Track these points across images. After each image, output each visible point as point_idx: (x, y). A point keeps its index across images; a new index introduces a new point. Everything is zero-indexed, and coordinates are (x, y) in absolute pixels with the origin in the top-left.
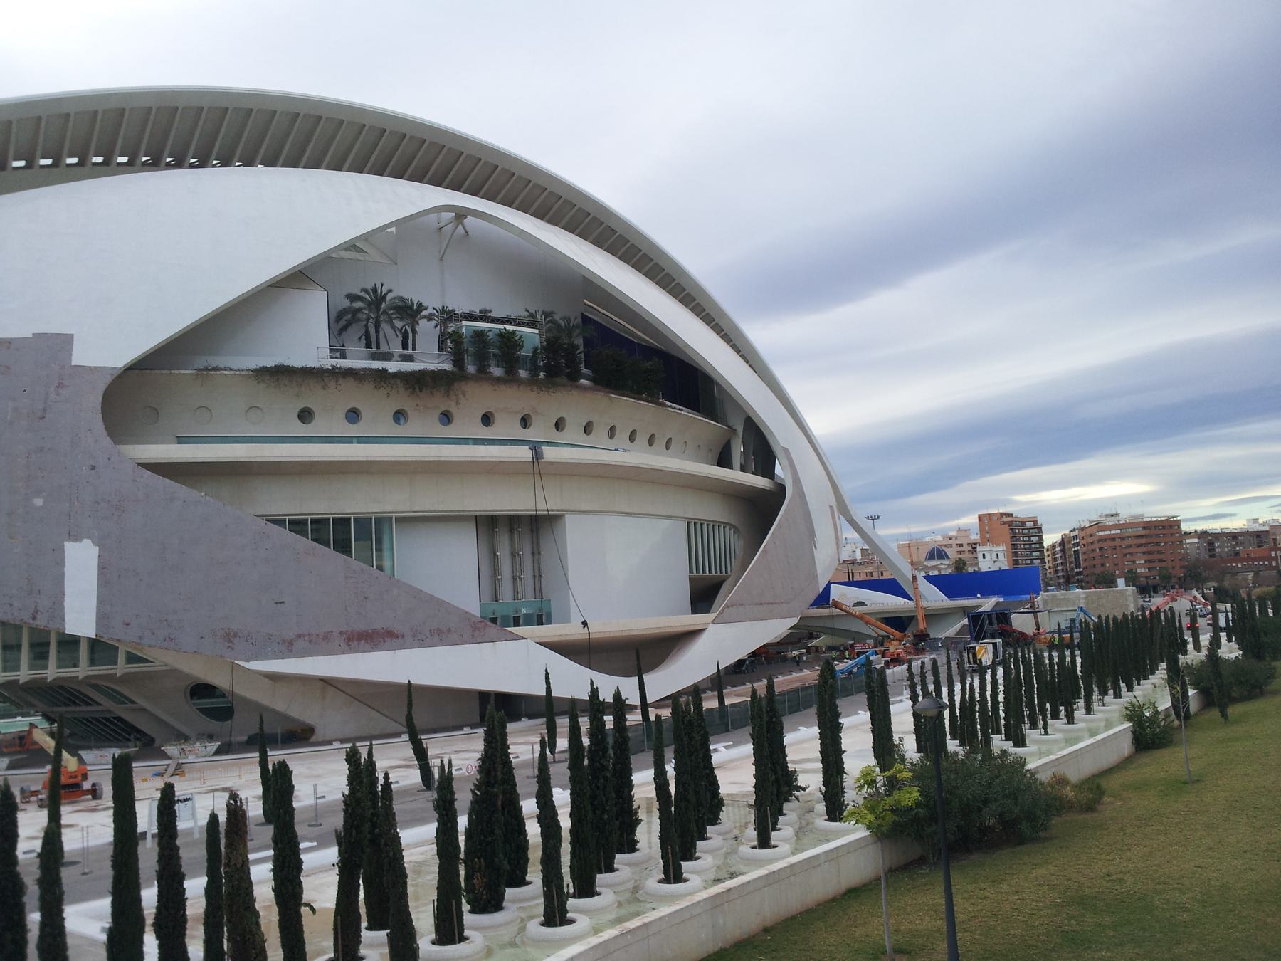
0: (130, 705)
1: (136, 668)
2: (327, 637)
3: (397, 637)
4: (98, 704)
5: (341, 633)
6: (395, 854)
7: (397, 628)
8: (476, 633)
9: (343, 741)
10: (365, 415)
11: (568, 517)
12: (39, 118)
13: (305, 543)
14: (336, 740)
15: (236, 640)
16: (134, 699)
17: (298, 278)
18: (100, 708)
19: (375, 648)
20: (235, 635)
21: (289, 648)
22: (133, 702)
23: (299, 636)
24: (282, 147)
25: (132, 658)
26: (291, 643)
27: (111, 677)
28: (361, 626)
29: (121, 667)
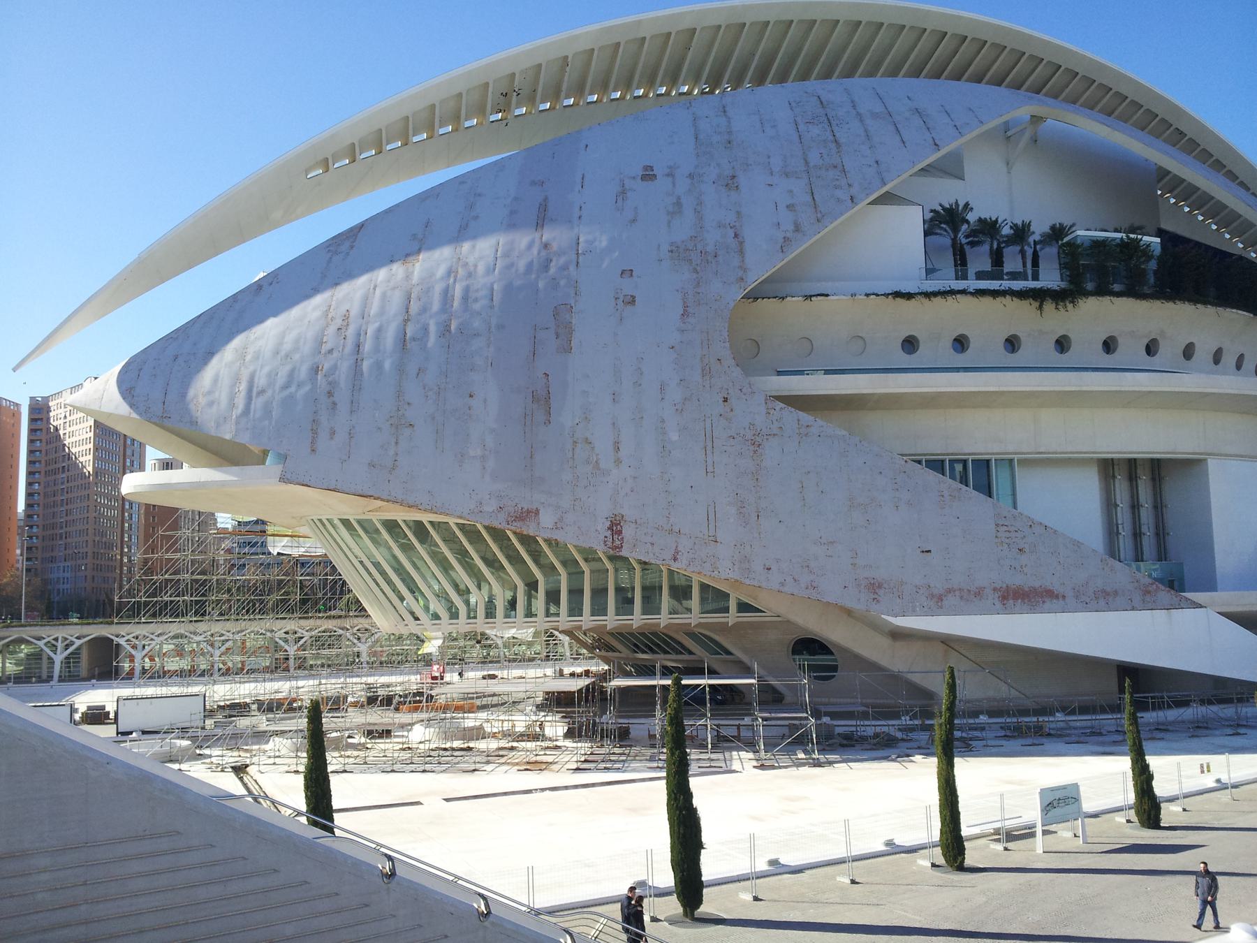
0: (725, 656)
1: (748, 617)
2: (979, 593)
3: (1057, 597)
4: (691, 653)
5: (995, 589)
6: (676, 799)
7: (1057, 588)
8: (1148, 598)
9: (116, 714)
10: (947, 342)
11: (1212, 464)
12: (567, 57)
13: (947, 484)
14: (982, 713)
15: (881, 592)
16: (694, 650)
17: (22, 626)
18: (692, 657)
19: (1033, 609)
20: (880, 586)
21: (938, 602)
22: (728, 653)
23: (949, 591)
24: (780, 46)
25: (744, 607)
26: (940, 598)
27: (723, 628)
28: (1017, 580)
29: (732, 617)
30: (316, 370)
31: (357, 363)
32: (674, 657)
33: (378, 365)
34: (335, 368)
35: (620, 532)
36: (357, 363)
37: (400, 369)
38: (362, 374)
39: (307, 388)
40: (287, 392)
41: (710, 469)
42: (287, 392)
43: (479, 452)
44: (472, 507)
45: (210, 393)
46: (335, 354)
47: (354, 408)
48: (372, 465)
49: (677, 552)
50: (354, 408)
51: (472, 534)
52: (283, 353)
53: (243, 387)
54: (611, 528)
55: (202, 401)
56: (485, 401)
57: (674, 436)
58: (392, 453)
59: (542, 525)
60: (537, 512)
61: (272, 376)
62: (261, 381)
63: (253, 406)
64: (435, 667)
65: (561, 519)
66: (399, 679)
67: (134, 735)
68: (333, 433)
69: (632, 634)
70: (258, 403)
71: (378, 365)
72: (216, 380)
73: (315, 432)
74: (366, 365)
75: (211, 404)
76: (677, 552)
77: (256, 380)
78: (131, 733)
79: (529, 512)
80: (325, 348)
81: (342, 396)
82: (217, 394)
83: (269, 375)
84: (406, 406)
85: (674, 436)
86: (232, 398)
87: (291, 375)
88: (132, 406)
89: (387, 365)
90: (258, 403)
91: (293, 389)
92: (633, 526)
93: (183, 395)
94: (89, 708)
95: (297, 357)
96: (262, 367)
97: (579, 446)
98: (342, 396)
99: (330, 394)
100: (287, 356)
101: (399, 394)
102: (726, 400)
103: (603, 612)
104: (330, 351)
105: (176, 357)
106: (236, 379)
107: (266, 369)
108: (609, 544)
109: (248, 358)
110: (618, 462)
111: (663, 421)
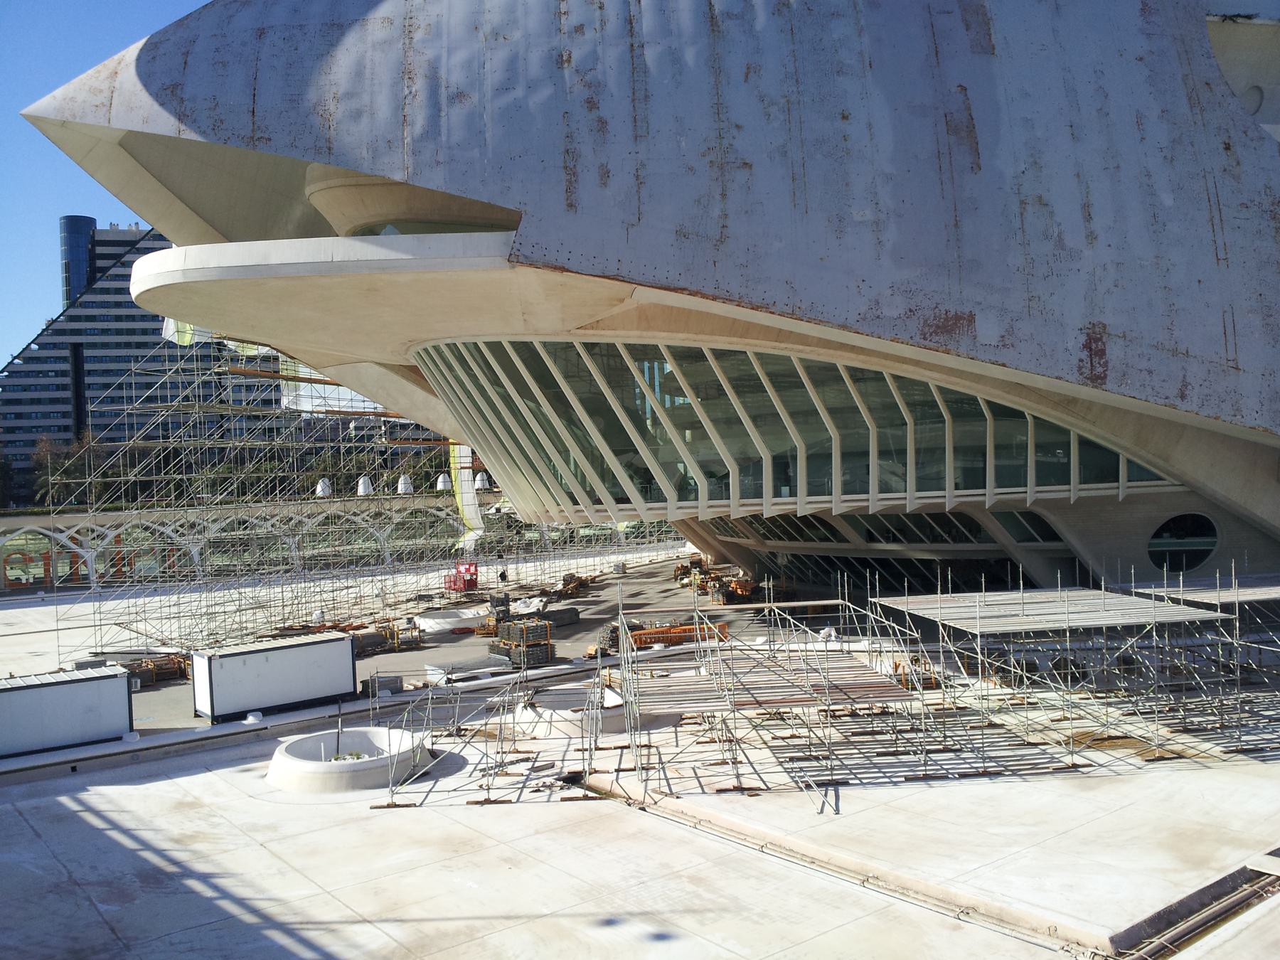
0: (1042, 544)
4: (844, 540)
27: (1060, 505)
30: (559, 60)
31: (634, 51)
32: (928, 545)
33: (674, 57)
34: (594, 57)
35: (1102, 353)
36: (634, 51)
37: (715, 66)
38: (646, 71)
39: (545, 92)
40: (507, 99)
41: (1221, 255)
42: (507, 99)
43: (869, 215)
44: (863, 309)
45: (349, 95)
46: (589, 34)
47: (640, 130)
48: (681, 234)
49: (1185, 385)
50: (640, 130)
51: (785, 379)
52: (487, 28)
53: (419, 85)
54: (1087, 346)
55: (337, 110)
56: (870, 126)
57: (1167, 200)
58: (716, 212)
59: (982, 339)
60: (971, 318)
61: (474, 67)
62: (454, 76)
63: (443, 120)
64: (764, 584)
65: (1010, 331)
66: (14, 543)
67: (251, 720)
68: (605, 174)
69: (868, 517)
70: (454, 116)
71: (674, 57)
72: (359, 73)
73: (572, 174)
74: (650, 55)
75: (357, 115)
76: (1185, 385)
77: (443, 73)
78: (242, 715)
79: (958, 318)
80: (567, 23)
81: (616, 108)
82: (366, 99)
83: (468, 64)
84: (734, 132)
85: (1167, 200)
86: (399, 106)
87: (512, 65)
88: (181, 117)
89: (690, 55)
90: (454, 116)
91: (519, 92)
92: (1121, 341)
93: (295, 100)
94: (268, 756)
95: (517, 35)
96: (450, 52)
97: (1029, 208)
98: (616, 108)
99: (591, 104)
100: (496, 34)
101: (719, 109)
102: (1228, 147)
103: (758, 494)
104: (579, 29)
105: (261, 33)
106: (404, 73)
107: (460, 56)
108: (1087, 372)
109: (418, 35)
110: (1091, 237)
111: (1149, 175)
